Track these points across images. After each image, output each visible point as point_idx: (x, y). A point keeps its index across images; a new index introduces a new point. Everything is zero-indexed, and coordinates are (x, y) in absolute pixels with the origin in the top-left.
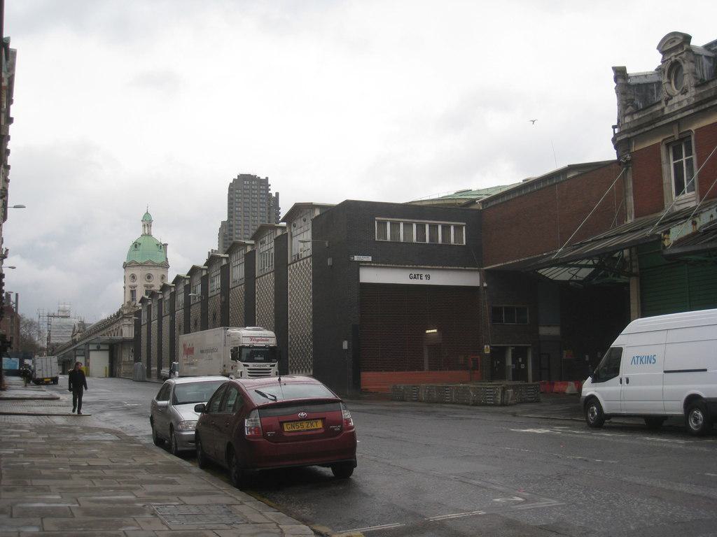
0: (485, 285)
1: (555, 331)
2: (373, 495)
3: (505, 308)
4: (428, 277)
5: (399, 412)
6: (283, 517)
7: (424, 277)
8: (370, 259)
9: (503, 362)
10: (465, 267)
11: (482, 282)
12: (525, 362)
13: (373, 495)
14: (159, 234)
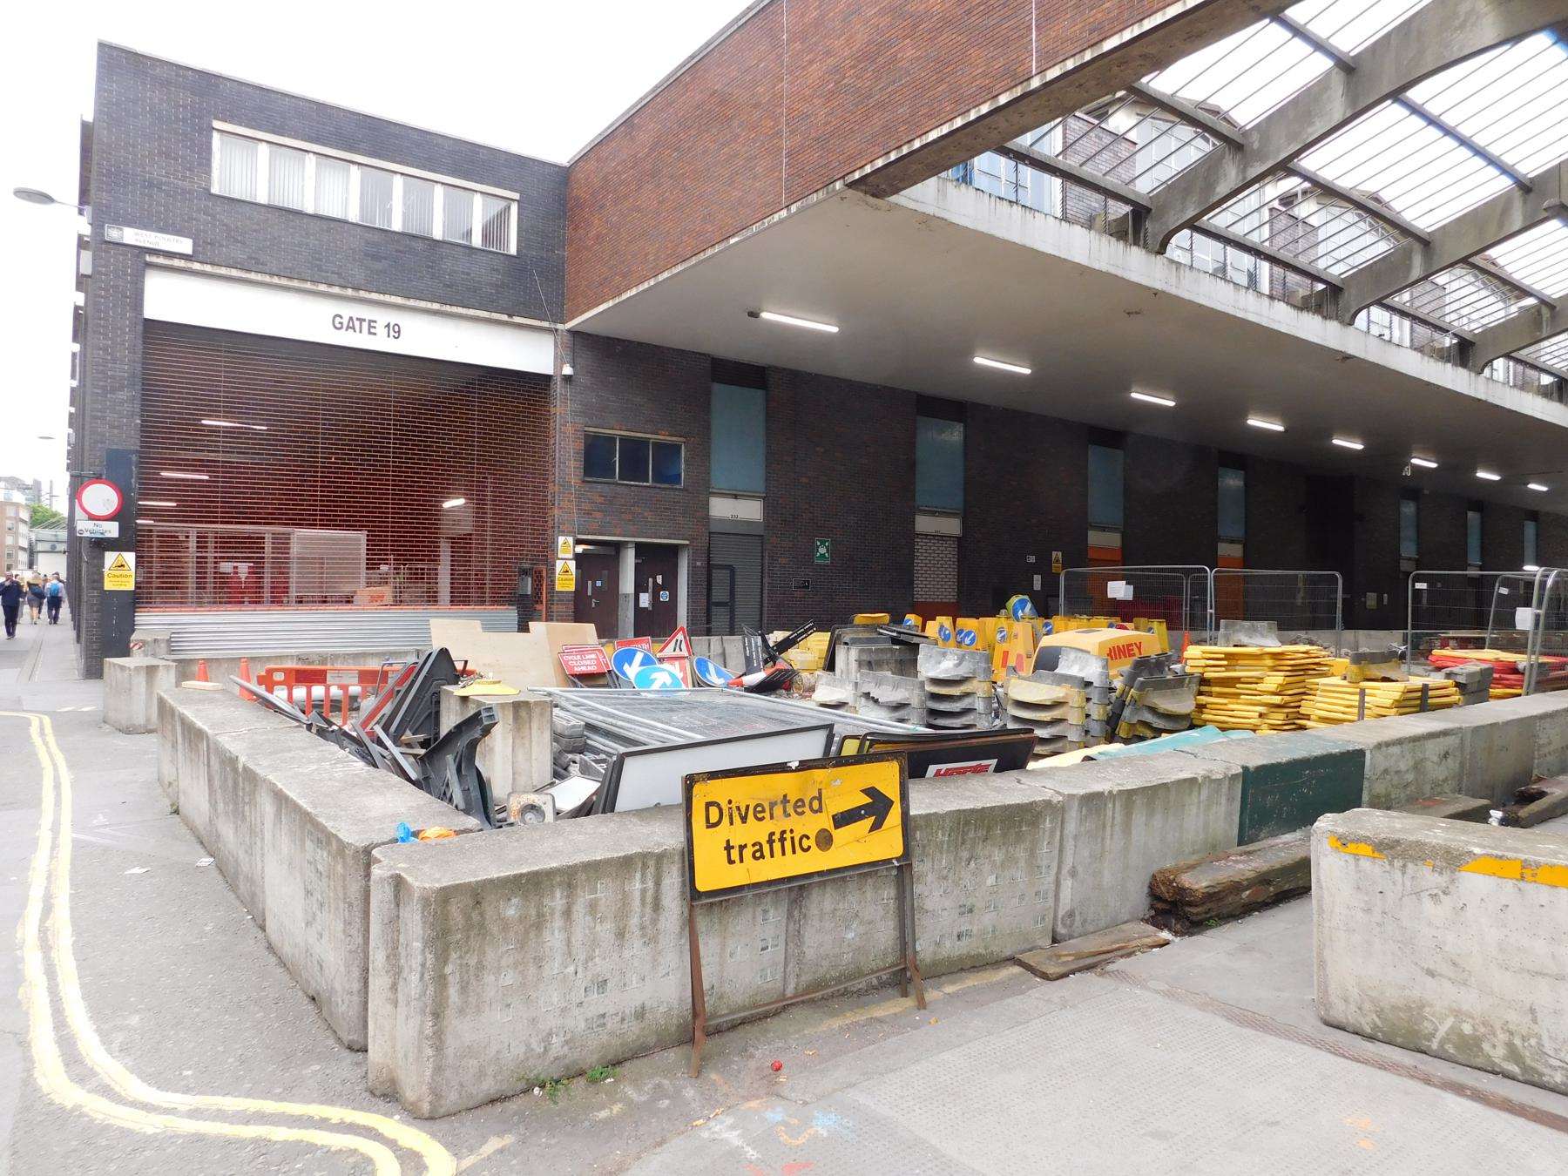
0: (567, 370)
1: (751, 511)
2: (643, 1007)
3: (624, 440)
4: (395, 331)
5: (683, 876)
6: (328, 818)
7: (380, 329)
8: (185, 245)
9: (614, 581)
10: (510, 316)
11: (558, 363)
12: (670, 584)
13: (643, 1007)
14: (909, 1002)
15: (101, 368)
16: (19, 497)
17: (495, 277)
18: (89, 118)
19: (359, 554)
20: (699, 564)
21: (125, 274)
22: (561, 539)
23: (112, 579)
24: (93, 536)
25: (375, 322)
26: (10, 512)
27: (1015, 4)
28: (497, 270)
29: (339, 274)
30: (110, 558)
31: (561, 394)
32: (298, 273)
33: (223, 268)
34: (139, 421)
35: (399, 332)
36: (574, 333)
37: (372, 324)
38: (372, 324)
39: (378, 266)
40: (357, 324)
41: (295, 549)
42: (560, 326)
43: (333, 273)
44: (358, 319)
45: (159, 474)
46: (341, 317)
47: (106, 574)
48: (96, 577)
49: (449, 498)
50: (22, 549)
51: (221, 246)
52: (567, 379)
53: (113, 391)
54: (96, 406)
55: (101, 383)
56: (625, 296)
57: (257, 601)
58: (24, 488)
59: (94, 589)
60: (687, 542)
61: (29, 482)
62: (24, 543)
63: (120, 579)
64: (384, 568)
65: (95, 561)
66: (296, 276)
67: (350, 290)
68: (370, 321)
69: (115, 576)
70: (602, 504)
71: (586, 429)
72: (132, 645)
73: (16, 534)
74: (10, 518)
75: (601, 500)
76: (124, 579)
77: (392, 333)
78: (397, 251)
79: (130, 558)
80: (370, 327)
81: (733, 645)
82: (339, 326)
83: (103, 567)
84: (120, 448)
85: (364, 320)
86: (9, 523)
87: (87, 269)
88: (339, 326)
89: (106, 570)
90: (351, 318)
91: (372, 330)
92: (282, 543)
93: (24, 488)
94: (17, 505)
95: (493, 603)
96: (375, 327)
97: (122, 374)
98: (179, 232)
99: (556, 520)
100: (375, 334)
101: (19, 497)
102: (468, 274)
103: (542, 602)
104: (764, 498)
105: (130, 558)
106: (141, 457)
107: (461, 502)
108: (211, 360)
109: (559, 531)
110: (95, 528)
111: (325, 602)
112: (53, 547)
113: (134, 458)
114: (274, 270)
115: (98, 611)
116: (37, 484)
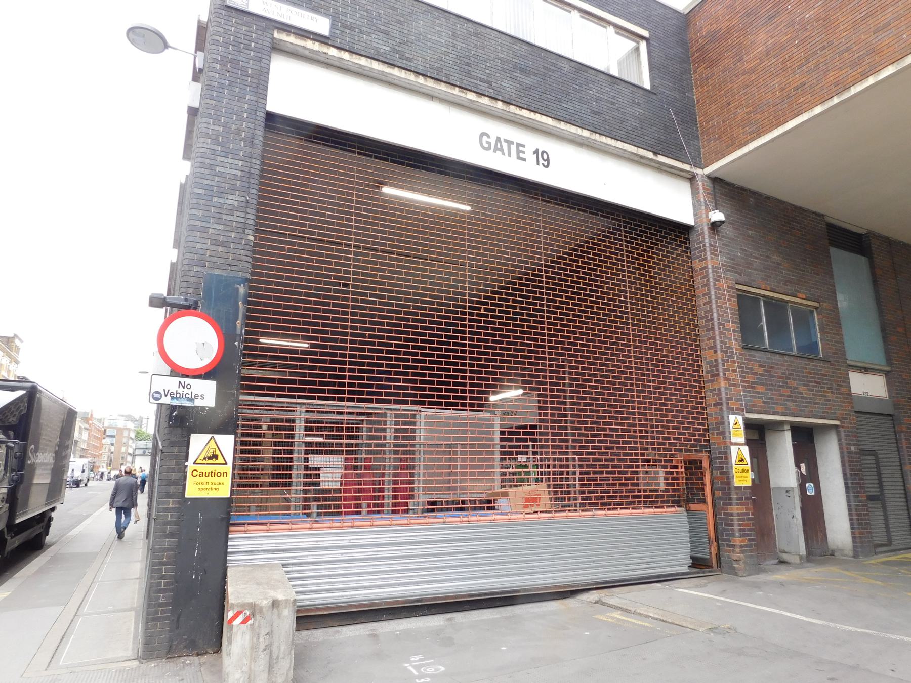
0: (717, 216)
4: (543, 159)
8: (321, 25)
10: (655, 154)
15: (208, 161)
16: (131, 425)
17: (638, 111)
18: (205, 18)
19: (492, 439)
20: (853, 448)
21: (247, 47)
22: (732, 418)
23: (198, 479)
24: (175, 402)
25: (524, 146)
26: (126, 433)
27: (880, 3)
28: (638, 104)
29: (489, 83)
30: (198, 443)
31: (710, 245)
32: (447, 75)
33: (363, 59)
34: (251, 238)
35: (548, 160)
36: (715, 180)
37: (521, 148)
38: (521, 148)
39: (528, 81)
40: (505, 145)
41: (421, 435)
42: (699, 171)
43: (482, 81)
44: (505, 141)
45: (257, 341)
46: (488, 136)
47: (189, 471)
48: (174, 476)
49: (501, 387)
50: (130, 454)
51: (361, 32)
52: (715, 226)
53: (221, 194)
54: (196, 212)
55: (206, 182)
56: (854, 90)
57: (377, 509)
58: (134, 421)
59: (169, 496)
60: (837, 423)
61: (137, 417)
62: (131, 451)
63: (209, 479)
64: (522, 459)
65: (175, 450)
66: (444, 79)
67: (500, 103)
68: (519, 145)
69: (202, 474)
70: (762, 375)
71: (738, 287)
72: (230, 614)
73: (127, 446)
74: (125, 437)
75: (760, 370)
76: (216, 479)
77: (541, 161)
78: (544, 68)
79: (226, 443)
80: (519, 152)
81: (72, 459)
82: (486, 145)
83: (187, 459)
84: (225, 274)
85: (512, 143)
86: (124, 440)
87: (199, 65)
88: (486, 145)
89: (190, 464)
90: (498, 139)
91: (521, 155)
92: (406, 429)
93: (134, 421)
94: (129, 430)
95: (589, 504)
96: (524, 152)
97: (234, 172)
98: (316, 9)
99: (723, 394)
100: (524, 160)
101: (131, 425)
102: (613, 104)
103: (704, 501)
104: (887, 374)
105: (226, 443)
106: (251, 288)
107: (514, 393)
108: (341, 174)
109: (729, 409)
110: (181, 390)
111: (462, 509)
112: (144, 452)
113: (242, 290)
114: (420, 69)
115: (172, 535)
116: (141, 418)
